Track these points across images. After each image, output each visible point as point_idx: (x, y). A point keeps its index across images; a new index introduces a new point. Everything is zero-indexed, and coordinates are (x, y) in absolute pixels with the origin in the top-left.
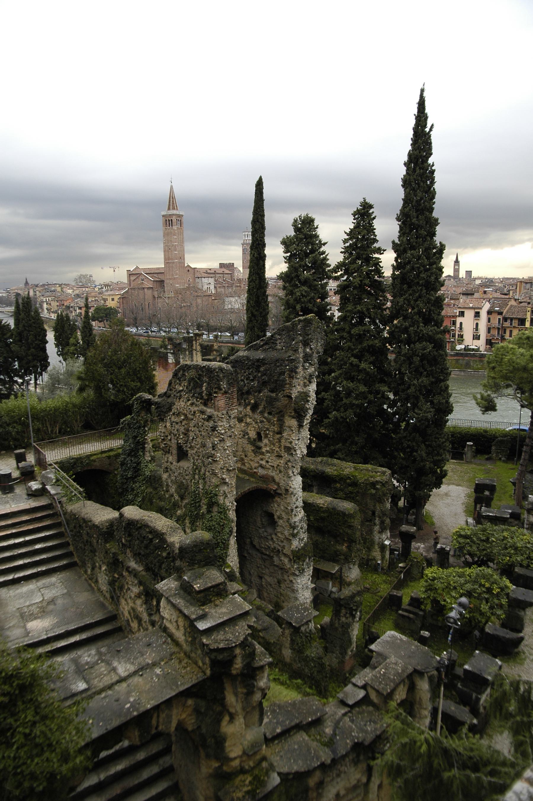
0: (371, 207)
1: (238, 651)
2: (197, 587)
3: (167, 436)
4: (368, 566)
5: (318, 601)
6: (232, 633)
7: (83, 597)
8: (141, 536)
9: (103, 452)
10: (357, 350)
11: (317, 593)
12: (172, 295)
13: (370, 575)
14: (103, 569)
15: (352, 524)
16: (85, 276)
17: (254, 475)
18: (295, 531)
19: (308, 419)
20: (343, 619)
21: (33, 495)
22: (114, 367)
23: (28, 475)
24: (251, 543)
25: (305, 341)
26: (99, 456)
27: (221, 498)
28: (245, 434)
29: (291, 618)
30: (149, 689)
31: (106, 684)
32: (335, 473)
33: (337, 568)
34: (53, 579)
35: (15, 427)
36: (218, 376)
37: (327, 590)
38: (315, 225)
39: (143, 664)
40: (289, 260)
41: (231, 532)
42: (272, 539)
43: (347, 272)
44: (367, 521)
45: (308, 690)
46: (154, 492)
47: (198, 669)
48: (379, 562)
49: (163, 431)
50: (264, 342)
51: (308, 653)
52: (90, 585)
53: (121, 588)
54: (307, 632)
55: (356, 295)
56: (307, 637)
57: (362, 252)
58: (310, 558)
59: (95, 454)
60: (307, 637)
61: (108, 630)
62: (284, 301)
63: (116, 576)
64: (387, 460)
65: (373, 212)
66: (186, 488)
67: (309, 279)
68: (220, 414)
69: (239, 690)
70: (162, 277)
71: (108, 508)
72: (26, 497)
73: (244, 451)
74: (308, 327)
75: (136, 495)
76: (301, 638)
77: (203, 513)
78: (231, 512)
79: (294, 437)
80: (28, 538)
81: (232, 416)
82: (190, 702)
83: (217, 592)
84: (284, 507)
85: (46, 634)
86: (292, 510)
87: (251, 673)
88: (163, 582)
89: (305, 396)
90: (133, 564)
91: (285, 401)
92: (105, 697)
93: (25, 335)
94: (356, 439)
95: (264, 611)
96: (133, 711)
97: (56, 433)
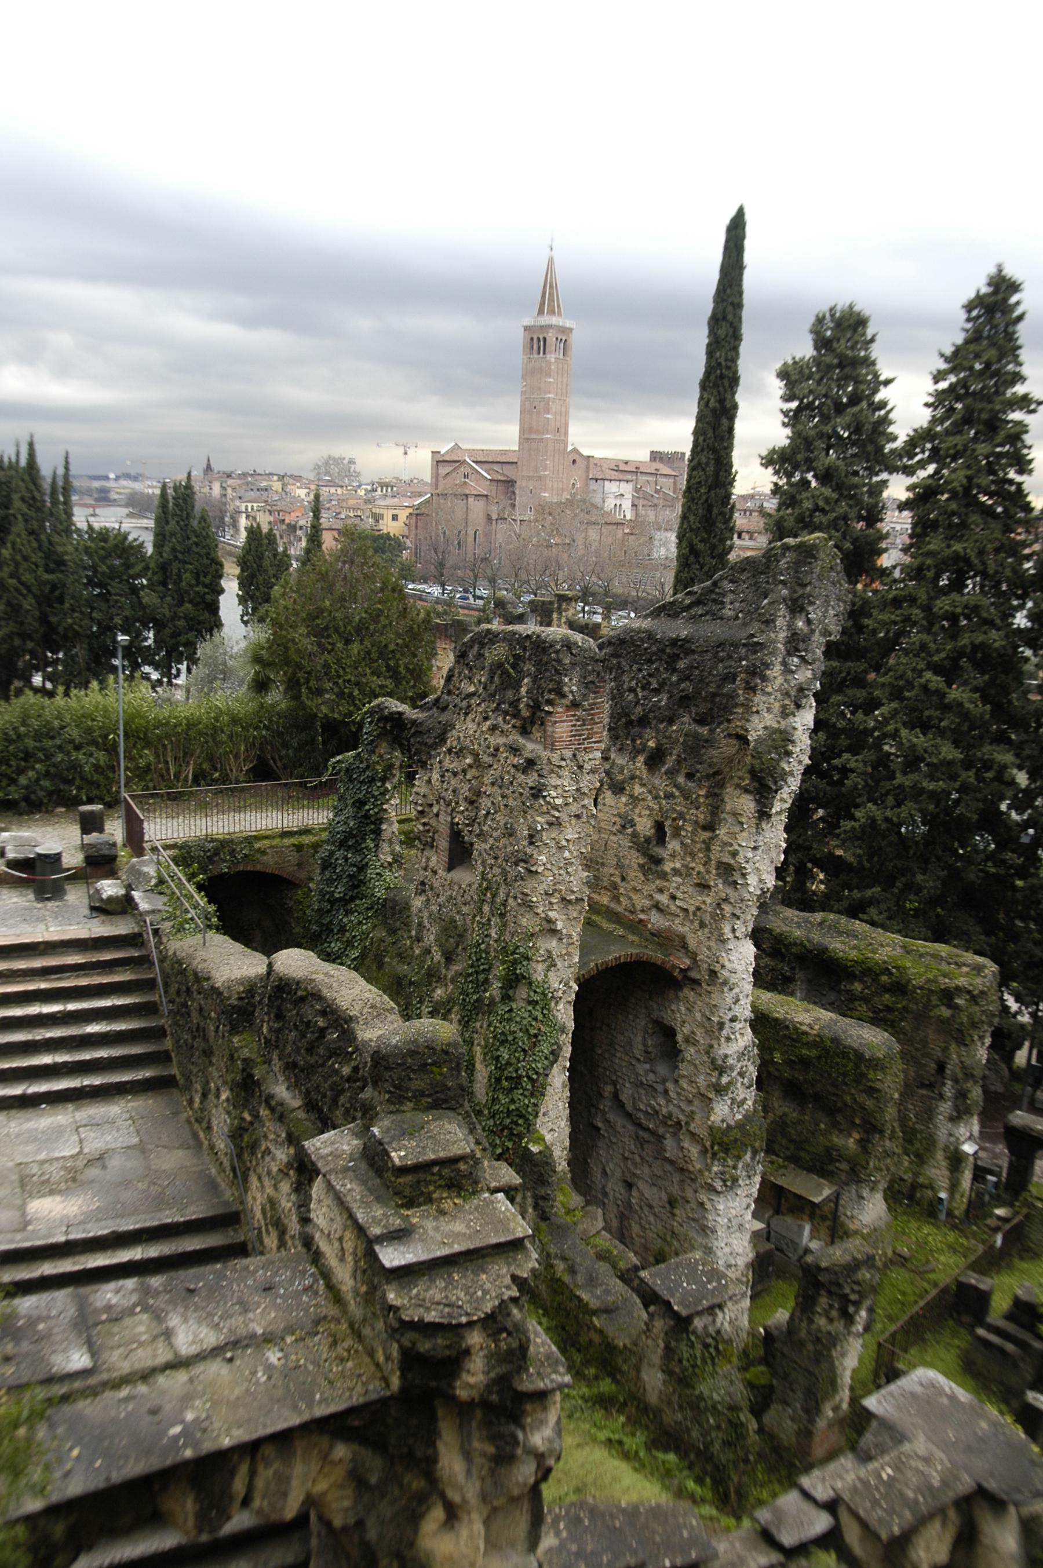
0: (1014, 287)
1: (475, 1338)
2: (397, 1156)
3: (431, 805)
4: (908, 1197)
5: (768, 1266)
6: (467, 1289)
7: (172, 1160)
8: (301, 1021)
9: (285, 834)
10: (943, 655)
11: (770, 1246)
12: (529, 515)
13: (914, 1224)
14: (223, 1097)
15: (878, 1085)
16: (338, 461)
17: (637, 927)
18: (725, 1080)
19: (783, 800)
20: (822, 1322)
21: (102, 909)
22: (335, 637)
23: (100, 863)
24: (616, 1096)
25: (795, 601)
26: (277, 841)
27: (540, 967)
28: (627, 823)
29: (671, 1291)
30: (238, 1398)
31: (138, 1366)
32: (854, 954)
33: (827, 1192)
34: (115, 1109)
35: (91, 755)
36: (559, 661)
37: (795, 1245)
38: (870, 333)
39: (242, 1332)
40: (793, 419)
41: (555, 1055)
42: (666, 1092)
43: (935, 456)
44: (923, 1086)
45: (691, 1485)
46: (390, 940)
47: (372, 1368)
48: (943, 1195)
49: (423, 791)
50: (693, 598)
51: (703, 1388)
52: (195, 1135)
53: (254, 1146)
54: (708, 1335)
55: (953, 513)
56: (706, 1346)
57: (979, 405)
58: (755, 1153)
59: (266, 837)
60: (706, 1346)
61: (198, 1245)
62: (771, 522)
63: (248, 1118)
64: (993, 939)
65: (1018, 303)
66: (461, 936)
67: (837, 469)
68: (555, 758)
69: (476, 1444)
70: (510, 472)
71: (257, 954)
72: (87, 912)
73: (619, 866)
74: (805, 564)
75: (349, 943)
76: (692, 1346)
77: (492, 999)
78: (561, 1006)
79: (744, 840)
80: (71, 1007)
81: (586, 766)
82: (341, 1451)
83: (452, 1178)
84: (703, 1015)
85: (67, 1233)
86: (721, 1025)
87: (508, 1407)
88: (325, 1136)
89: (782, 740)
90: (281, 1091)
91: (729, 747)
92: (127, 1399)
93: (175, 571)
94: (920, 878)
95: (614, 1267)
96: (185, 1446)
97: (186, 780)
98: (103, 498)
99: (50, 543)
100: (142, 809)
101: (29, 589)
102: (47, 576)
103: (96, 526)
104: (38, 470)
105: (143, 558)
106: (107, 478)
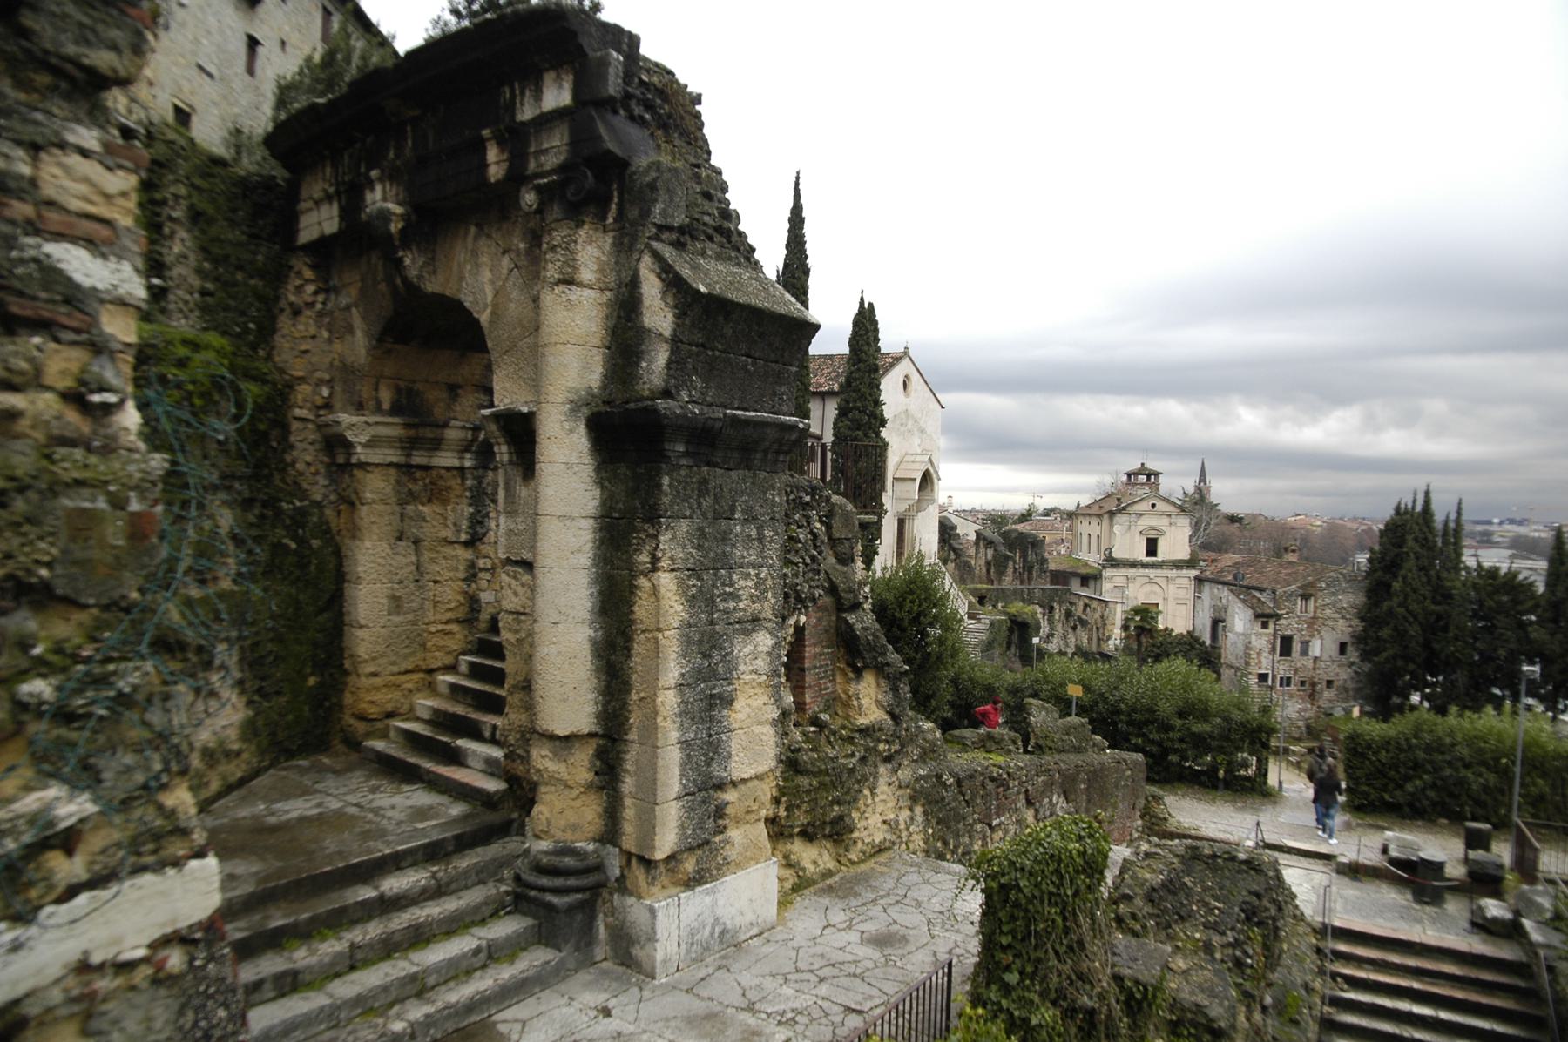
21: (1483, 926)
23: (1483, 881)
35: (1480, 775)
72: (1466, 925)
80: (1444, 1015)
98: (1486, 540)
99: (1439, 578)
100: (1538, 840)
101: (1415, 617)
102: (1433, 607)
103: (1486, 565)
104: (1432, 515)
105: (1533, 596)
106: (1489, 523)
